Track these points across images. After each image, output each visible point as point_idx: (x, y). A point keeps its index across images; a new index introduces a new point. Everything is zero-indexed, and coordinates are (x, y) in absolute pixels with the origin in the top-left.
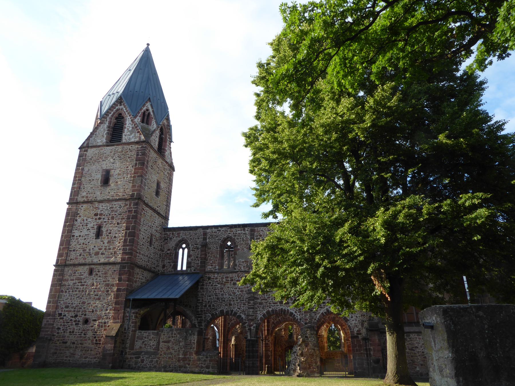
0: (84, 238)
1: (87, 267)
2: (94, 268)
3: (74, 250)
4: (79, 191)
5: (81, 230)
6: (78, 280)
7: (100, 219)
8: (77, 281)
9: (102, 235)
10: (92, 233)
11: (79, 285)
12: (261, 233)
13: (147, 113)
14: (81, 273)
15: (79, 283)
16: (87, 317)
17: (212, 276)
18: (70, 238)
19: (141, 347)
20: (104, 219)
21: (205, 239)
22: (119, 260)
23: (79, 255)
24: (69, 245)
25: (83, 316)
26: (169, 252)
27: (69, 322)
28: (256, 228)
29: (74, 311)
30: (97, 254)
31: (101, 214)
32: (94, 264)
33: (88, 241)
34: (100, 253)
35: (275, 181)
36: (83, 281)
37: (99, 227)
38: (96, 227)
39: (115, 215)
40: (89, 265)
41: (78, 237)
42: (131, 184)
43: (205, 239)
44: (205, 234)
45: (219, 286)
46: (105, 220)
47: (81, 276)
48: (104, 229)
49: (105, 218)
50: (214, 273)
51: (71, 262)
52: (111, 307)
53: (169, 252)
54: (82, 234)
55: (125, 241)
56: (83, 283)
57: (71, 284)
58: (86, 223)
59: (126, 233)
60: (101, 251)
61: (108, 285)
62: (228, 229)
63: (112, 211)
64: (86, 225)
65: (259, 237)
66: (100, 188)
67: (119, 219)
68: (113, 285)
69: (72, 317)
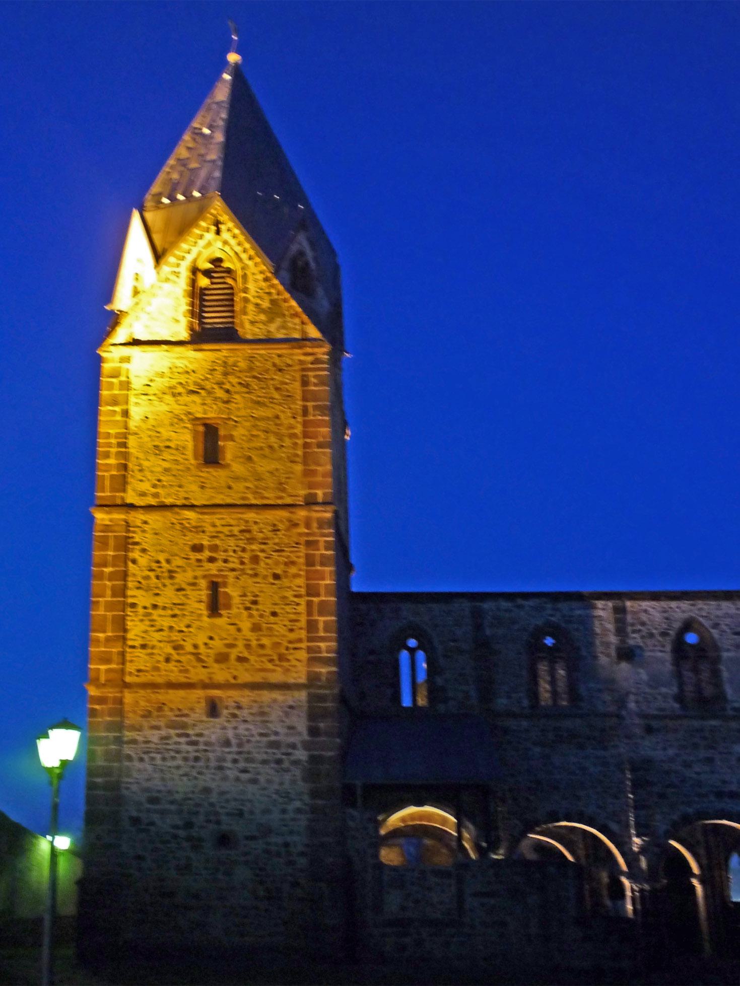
0: (170, 612)
1: (200, 693)
2: (220, 698)
3: (144, 646)
4: (124, 477)
5: (157, 591)
6: (174, 728)
7: (212, 560)
8: (172, 732)
9: (228, 606)
10: (198, 600)
11: (179, 743)
12: (644, 617)
13: (300, 263)
14: (179, 710)
15: (179, 735)
16: (224, 827)
17: (511, 723)
18: (124, 611)
19: (403, 908)
20: (225, 561)
21: (479, 627)
22: (300, 675)
23: (161, 659)
24: (125, 630)
25: (212, 826)
26: (371, 658)
27: (168, 842)
28: (628, 604)
29: (180, 812)
30: (222, 658)
31: (214, 548)
32: (218, 686)
33: (186, 621)
34: (233, 657)
35: (187, 441)
36: (190, 732)
37: (214, 587)
38: (203, 583)
39: (263, 551)
40: (205, 686)
41: (150, 611)
42: (299, 468)
43: (479, 627)
44: (477, 614)
45: (537, 750)
46: (231, 565)
47: (184, 719)
48: (232, 591)
49: (231, 559)
50: (514, 716)
51: (143, 679)
52: (298, 804)
53: (371, 658)
54: (160, 601)
55: (311, 626)
56: (194, 738)
57: (155, 739)
58: (170, 571)
59: (309, 604)
60: (234, 653)
61: (275, 745)
62: (546, 603)
63: (251, 540)
64: (171, 577)
65: (639, 627)
66: (194, 471)
67: (277, 563)
68: (293, 746)
69: (176, 827)
